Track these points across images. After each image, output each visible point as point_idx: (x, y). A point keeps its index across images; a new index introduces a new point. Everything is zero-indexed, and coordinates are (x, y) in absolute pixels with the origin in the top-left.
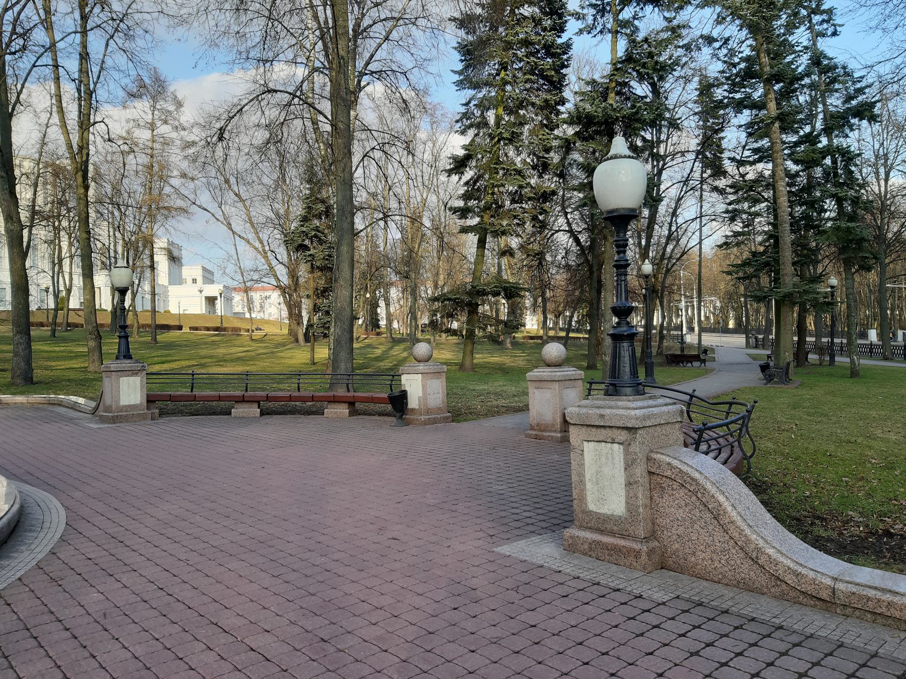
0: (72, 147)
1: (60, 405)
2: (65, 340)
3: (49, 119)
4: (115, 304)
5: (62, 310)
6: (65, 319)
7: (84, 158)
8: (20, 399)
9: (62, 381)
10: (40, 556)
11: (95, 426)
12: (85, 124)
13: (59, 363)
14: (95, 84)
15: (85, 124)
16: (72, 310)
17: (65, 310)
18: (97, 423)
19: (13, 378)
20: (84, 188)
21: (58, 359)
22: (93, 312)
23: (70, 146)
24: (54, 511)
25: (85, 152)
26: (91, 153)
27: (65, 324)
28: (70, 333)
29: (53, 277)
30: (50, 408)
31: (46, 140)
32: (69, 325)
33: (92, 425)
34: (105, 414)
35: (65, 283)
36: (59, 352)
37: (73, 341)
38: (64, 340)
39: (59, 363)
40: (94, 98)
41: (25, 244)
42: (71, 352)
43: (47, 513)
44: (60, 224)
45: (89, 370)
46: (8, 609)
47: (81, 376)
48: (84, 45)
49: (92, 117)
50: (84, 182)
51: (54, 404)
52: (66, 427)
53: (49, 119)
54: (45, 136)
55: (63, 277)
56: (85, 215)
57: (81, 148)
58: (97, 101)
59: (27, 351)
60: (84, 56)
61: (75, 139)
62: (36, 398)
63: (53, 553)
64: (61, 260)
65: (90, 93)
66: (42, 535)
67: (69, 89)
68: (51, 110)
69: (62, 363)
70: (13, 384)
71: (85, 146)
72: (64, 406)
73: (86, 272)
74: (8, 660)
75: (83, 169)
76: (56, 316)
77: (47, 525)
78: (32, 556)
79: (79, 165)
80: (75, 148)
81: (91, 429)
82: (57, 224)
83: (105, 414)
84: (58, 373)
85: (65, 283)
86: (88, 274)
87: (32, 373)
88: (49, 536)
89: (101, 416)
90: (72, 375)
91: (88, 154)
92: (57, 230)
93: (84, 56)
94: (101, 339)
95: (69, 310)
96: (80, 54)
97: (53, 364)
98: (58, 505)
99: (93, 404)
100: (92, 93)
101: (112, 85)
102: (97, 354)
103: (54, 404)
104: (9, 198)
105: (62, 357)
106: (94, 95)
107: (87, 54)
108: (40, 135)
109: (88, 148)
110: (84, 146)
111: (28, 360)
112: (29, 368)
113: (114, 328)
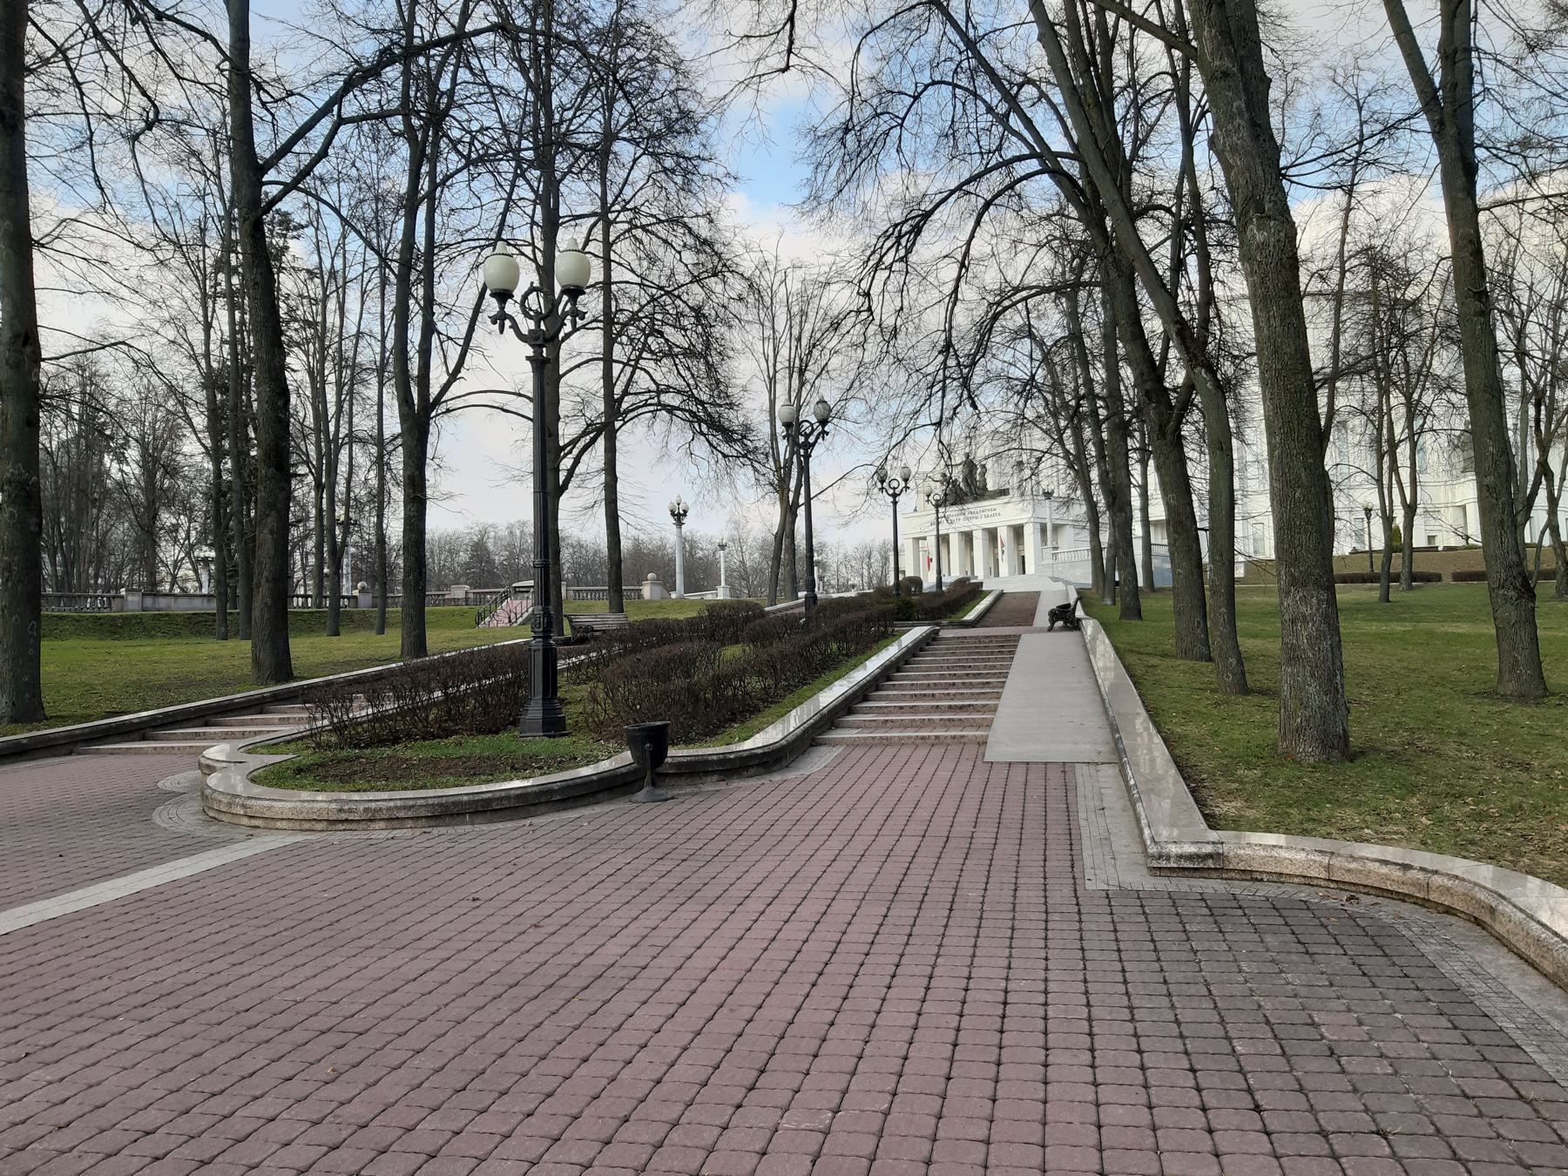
16: (1419, 550)
59: (1326, 645)
64: (1393, 445)
70: (1288, 757)
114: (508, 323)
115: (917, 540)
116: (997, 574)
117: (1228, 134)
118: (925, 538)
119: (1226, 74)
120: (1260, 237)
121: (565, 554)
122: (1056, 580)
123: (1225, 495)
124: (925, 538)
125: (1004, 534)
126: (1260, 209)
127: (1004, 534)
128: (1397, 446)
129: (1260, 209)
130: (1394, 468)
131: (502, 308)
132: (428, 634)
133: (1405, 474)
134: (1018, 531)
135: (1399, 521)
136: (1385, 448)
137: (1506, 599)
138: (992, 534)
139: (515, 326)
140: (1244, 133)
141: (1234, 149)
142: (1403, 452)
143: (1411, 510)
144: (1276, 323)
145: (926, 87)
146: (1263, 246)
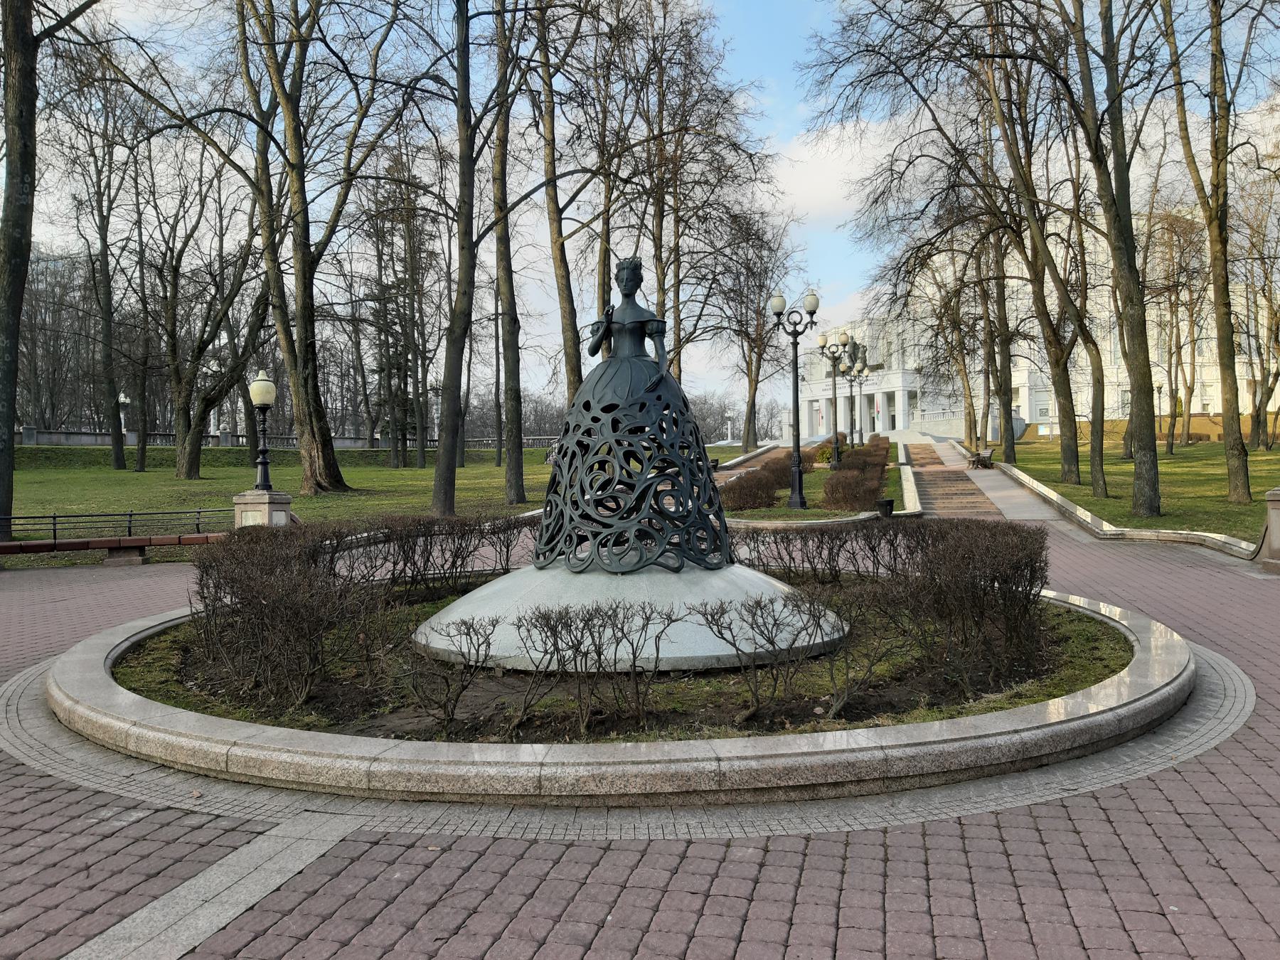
0: (1203, 188)
1: (1201, 545)
2: (1187, 458)
3: (1162, 155)
4: (1257, 403)
5: (1181, 415)
6: (1186, 428)
7: (1221, 201)
8: (1147, 534)
9: (1198, 512)
10: (1234, 728)
11: (1260, 577)
12: (1221, 150)
13: (1186, 490)
14: (1234, 92)
15: (1221, 150)
16: (1195, 415)
17: (1186, 417)
18: (1260, 573)
19: (1135, 506)
20: (1221, 242)
21: (1183, 483)
22: (1236, 417)
23: (1200, 187)
24: (1235, 677)
25: (1221, 191)
26: (1230, 190)
27: (1185, 436)
28: (1192, 449)
29: (1169, 372)
30: (1189, 548)
31: (1159, 185)
32: (1190, 437)
33: (1254, 575)
34: (1271, 561)
35: (1185, 380)
36: (1182, 474)
37: (1198, 459)
38: (1185, 458)
39: (1186, 490)
40: (1232, 112)
41: (476, 149)
42: (1199, 475)
43: (1226, 679)
44: (1178, 298)
45: (1229, 499)
46: (1213, 778)
47: (1221, 508)
48: (1217, 40)
49: (1230, 139)
50: (1221, 234)
51: (1194, 544)
52: (1219, 575)
53: (1162, 155)
54: (1157, 180)
55: (1183, 370)
56: (1223, 281)
57: (1216, 187)
58: (1236, 115)
59: (1152, 473)
60: (1218, 57)
61: (1207, 175)
62: (1166, 533)
63: (1248, 727)
64: (1179, 348)
65: (1227, 106)
66: (1228, 704)
67: (1199, 110)
68: (1165, 142)
69: (1191, 489)
70: (1135, 515)
71: (1222, 183)
72: (1207, 547)
73: (1225, 360)
74: (934, 941)
75: (1220, 217)
76: (1173, 425)
77: (1230, 693)
78: (1223, 726)
79: (1214, 212)
80: (1208, 190)
81: (1254, 579)
82: (1173, 298)
83: (1271, 561)
84: (1189, 503)
85: (1185, 380)
86: (1227, 364)
87: (1159, 501)
88: (1238, 706)
89: (1265, 564)
90: (1209, 506)
91: (1226, 194)
92: (1174, 307)
93: (1218, 57)
94: (1246, 455)
95: (1190, 416)
96: (1213, 55)
97: (1178, 490)
98: (1238, 670)
99: (1252, 547)
100: (1229, 105)
101: (1259, 82)
102: (1241, 477)
103: (1194, 544)
104: (1128, 275)
105: (1188, 481)
106: (1232, 107)
107: (1222, 52)
108: (1150, 181)
109: (1226, 186)
110: (1220, 184)
111: (1154, 482)
112: (1155, 494)
113: (1256, 440)
114: (781, 327)
115: (811, 402)
116: (894, 427)
117: (1120, 271)
118: (817, 401)
119: (1120, 248)
120: (1131, 312)
121: (527, 408)
122: (924, 434)
123: (1100, 409)
124: (817, 401)
125: (880, 400)
126: (1132, 301)
127: (880, 400)
128: (1181, 348)
129: (1132, 301)
130: (1179, 363)
131: (779, 320)
132: (525, 469)
133: (1187, 369)
134: (890, 397)
135: (1182, 394)
136: (1174, 349)
137: (1233, 455)
138: (870, 399)
139: (784, 328)
140: (1126, 271)
141: (1122, 277)
142: (1186, 351)
143: (1190, 390)
144: (1137, 346)
145: (917, 157)
146: (1132, 316)
